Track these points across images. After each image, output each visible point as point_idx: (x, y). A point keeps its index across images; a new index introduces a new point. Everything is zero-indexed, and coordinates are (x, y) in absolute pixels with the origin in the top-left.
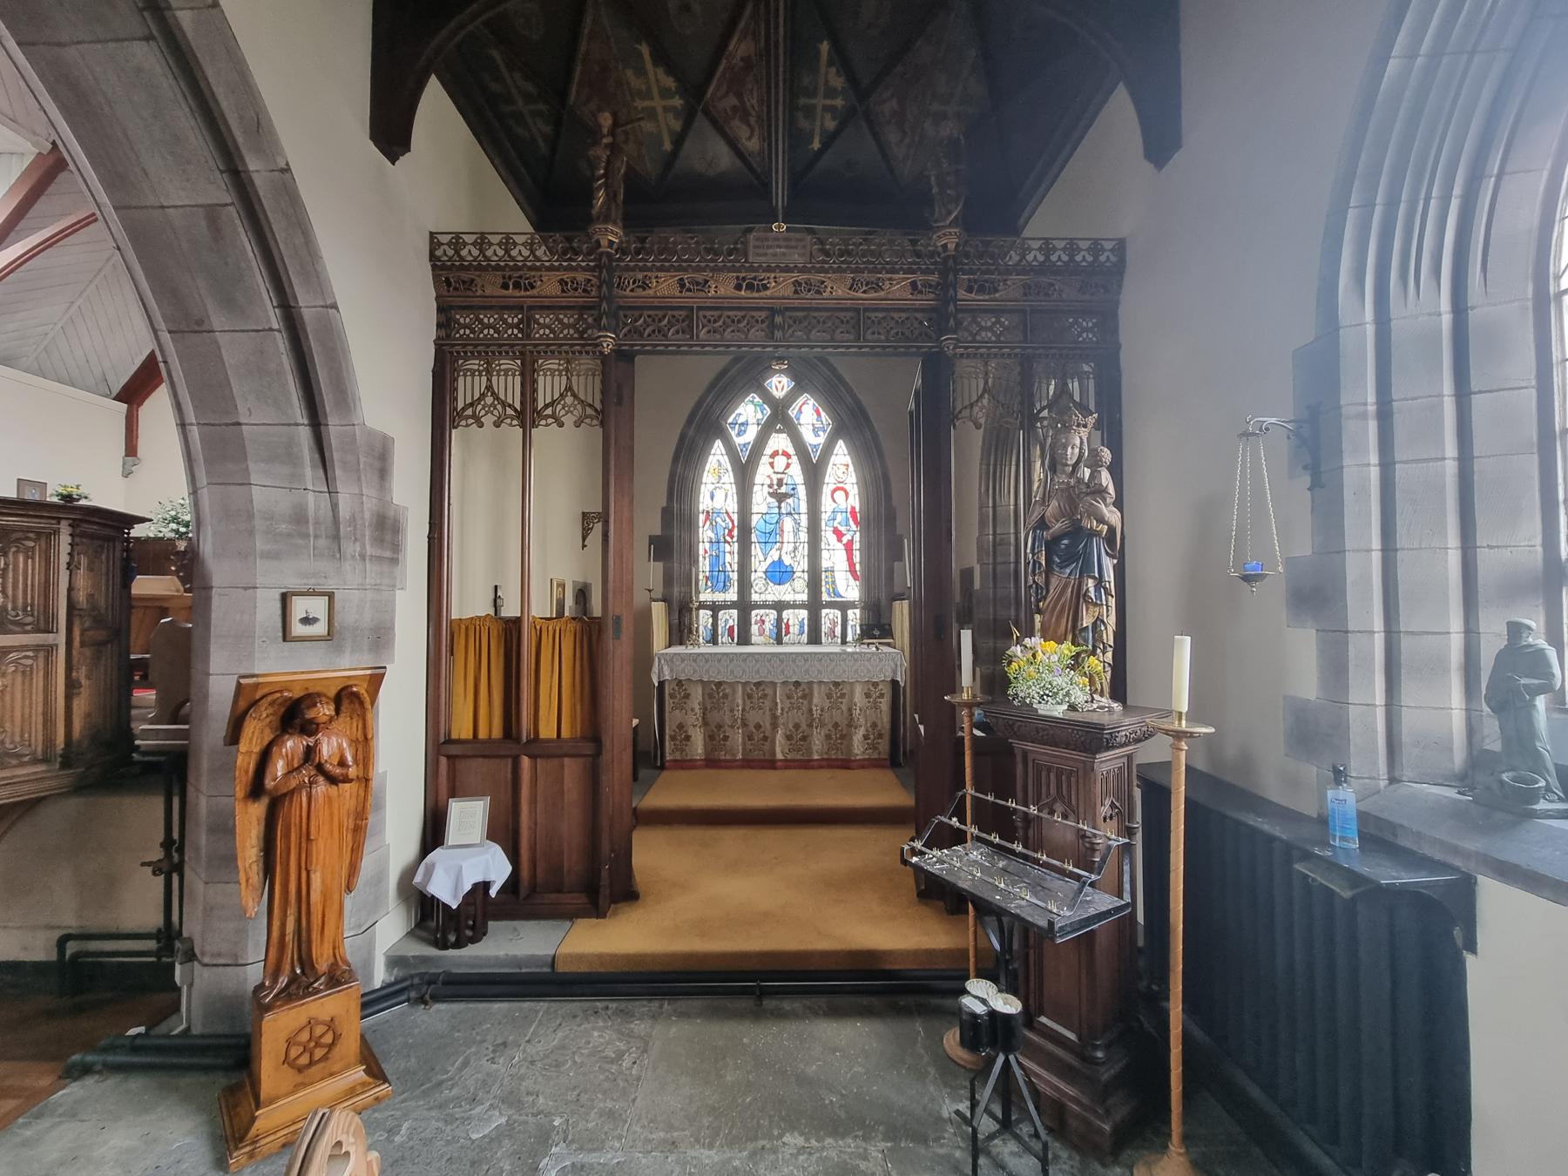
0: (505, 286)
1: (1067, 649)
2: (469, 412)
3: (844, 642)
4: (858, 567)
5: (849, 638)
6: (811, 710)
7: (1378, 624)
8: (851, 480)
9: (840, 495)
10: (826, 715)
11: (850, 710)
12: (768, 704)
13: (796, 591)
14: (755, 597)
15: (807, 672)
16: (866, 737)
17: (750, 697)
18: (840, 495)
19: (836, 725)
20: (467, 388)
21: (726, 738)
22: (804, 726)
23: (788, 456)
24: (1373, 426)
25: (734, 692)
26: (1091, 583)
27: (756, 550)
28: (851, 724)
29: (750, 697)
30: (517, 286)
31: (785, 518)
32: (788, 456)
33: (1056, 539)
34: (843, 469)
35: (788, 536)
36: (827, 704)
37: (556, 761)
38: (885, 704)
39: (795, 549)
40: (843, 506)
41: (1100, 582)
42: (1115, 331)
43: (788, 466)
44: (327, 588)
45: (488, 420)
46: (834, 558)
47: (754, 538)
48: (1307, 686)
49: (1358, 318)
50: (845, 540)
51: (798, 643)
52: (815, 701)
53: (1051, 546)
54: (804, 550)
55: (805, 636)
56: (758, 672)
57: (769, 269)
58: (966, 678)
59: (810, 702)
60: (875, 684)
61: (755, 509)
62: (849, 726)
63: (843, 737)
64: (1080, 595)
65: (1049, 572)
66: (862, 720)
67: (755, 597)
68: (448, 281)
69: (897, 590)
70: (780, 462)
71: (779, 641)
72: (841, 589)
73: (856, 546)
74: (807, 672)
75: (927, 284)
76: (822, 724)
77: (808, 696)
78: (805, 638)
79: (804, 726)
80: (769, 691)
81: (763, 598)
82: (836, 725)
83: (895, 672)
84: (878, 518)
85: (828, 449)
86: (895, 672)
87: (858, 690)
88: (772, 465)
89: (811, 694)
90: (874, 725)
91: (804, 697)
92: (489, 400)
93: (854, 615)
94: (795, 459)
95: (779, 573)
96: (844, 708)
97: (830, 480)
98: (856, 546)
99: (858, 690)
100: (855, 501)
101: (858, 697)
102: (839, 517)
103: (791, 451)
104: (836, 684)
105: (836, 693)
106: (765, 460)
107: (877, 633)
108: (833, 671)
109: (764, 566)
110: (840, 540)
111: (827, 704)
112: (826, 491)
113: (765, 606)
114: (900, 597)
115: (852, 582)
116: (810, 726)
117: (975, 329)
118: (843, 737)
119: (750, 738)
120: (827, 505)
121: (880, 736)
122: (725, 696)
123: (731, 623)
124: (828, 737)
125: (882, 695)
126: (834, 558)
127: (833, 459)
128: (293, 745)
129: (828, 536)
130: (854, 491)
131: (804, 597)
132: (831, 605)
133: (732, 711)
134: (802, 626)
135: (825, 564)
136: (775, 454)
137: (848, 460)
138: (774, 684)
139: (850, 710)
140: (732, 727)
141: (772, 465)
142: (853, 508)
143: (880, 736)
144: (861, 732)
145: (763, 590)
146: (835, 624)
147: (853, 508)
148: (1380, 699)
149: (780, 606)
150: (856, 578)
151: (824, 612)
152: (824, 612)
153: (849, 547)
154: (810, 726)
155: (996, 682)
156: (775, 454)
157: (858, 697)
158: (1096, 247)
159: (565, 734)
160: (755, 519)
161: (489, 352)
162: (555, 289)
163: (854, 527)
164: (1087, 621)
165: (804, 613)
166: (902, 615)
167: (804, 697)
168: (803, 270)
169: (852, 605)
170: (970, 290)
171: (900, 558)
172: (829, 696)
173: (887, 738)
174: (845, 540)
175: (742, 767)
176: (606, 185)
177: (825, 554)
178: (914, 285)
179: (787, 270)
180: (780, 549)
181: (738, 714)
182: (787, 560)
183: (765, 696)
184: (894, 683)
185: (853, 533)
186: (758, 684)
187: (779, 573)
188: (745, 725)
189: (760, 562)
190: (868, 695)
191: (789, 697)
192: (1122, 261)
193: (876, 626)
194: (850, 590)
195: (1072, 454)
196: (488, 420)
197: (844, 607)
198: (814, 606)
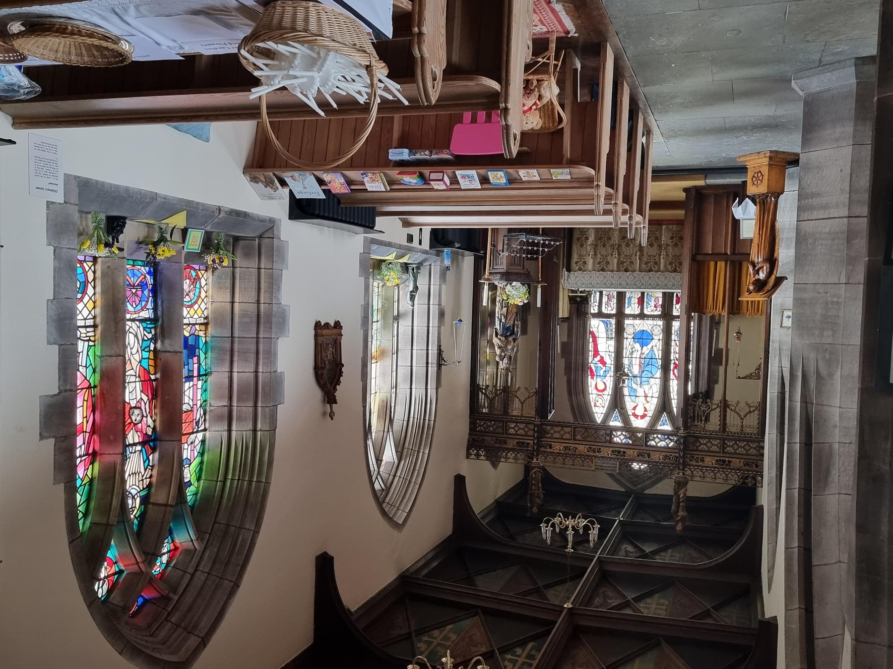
0: (729, 462)
1: (511, 301)
2: (752, 409)
3: (601, 293)
4: (591, 340)
5: (598, 294)
6: (619, 255)
7: (431, 307)
8: (593, 396)
9: (601, 387)
10: (610, 252)
11: (595, 255)
12: (645, 259)
13: (632, 326)
14: (660, 323)
15: (620, 277)
16: (587, 238)
17: (656, 263)
18: (601, 387)
19: (604, 246)
20: (752, 420)
21: (672, 238)
22: (623, 245)
23: (636, 416)
24: (430, 361)
25: (665, 266)
26: (503, 320)
27: (658, 354)
28: (595, 246)
29: (656, 263)
30: (724, 461)
31: (632, 372)
32: (636, 416)
33: (511, 335)
34: (598, 404)
35: (636, 362)
36: (609, 258)
37: (715, 252)
38: (575, 257)
39: (632, 353)
40: (599, 380)
41: (500, 321)
42: (471, 423)
43: (634, 408)
44: (782, 330)
45: (742, 404)
46: (606, 347)
47: (660, 362)
48: (443, 286)
49: (431, 392)
50: (598, 358)
51: (632, 296)
52: (616, 261)
53: (513, 333)
54: (626, 353)
55: (627, 296)
56: (650, 278)
57: (611, 458)
58: (539, 290)
59: (619, 260)
60: (580, 269)
61: (658, 381)
62: (596, 245)
63: (601, 238)
64: (506, 318)
65: (514, 325)
66: (589, 248)
67: (660, 323)
68: (757, 466)
69: (566, 325)
70: (640, 411)
71: (643, 294)
72: (602, 327)
73: (591, 354)
74: (620, 277)
75: (546, 448)
76: (612, 246)
77: (620, 263)
78: (628, 295)
79: (623, 245)
80: (644, 266)
81: (655, 322)
82: (604, 246)
83: (568, 277)
84: (578, 372)
85: (607, 416)
86: (568, 277)
87: (590, 266)
88: (646, 410)
89: (618, 264)
90: (582, 245)
91: (623, 263)
92: (742, 414)
93: (594, 309)
94: (630, 413)
95: (643, 338)
96: (599, 256)
97: (607, 398)
98: (591, 354)
99: (590, 266)
100: (591, 382)
101: (590, 262)
102: (602, 373)
103: (632, 418)
104: (603, 270)
105: (603, 265)
106: (650, 413)
107: (578, 299)
108: (605, 278)
109: (653, 343)
110: (602, 358)
111: (609, 258)
112: (609, 391)
113: (654, 317)
114: (564, 320)
115: (594, 330)
116: (620, 245)
117: (526, 429)
118: (601, 238)
119: (657, 238)
120: (610, 382)
121: (578, 239)
122: (671, 263)
123: (678, 306)
124: (609, 239)
125: (577, 263)
126: (606, 347)
127: (604, 411)
128: (762, 276)
129: (610, 361)
130: (591, 389)
131: (627, 322)
132: (609, 316)
133: (667, 255)
134: (629, 302)
135: (612, 343)
136: (643, 417)
137: (595, 410)
138: (640, 271)
139: (595, 255)
140: (667, 245)
141: (646, 410)
142: (592, 378)
143: (578, 239)
144: (590, 241)
145: (655, 327)
146: (607, 304)
147: (592, 378)
148: (432, 286)
149: (642, 316)
150: (592, 333)
151: (614, 312)
152: (614, 312)
153: (596, 353)
154: (620, 245)
155: (532, 293)
156: (643, 417)
157: (590, 262)
158: (478, 456)
159: (712, 264)
160: (658, 374)
161: (740, 437)
162: (707, 459)
163: (592, 366)
164: (505, 309)
165: (628, 311)
166: (563, 309)
167: (623, 263)
168: (596, 457)
169: (595, 316)
170: (528, 444)
171: (563, 344)
172: (608, 263)
173: (575, 239)
174: (598, 358)
175: (662, 220)
176: (679, 498)
177: (612, 349)
178: (551, 447)
179: (603, 457)
180: (642, 354)
181: (663, 253)
182: (637, 346)
183: (646, 263)
184: (569, 270)
185: (593, 362)
186: (650, 271)
187: (643, 338)
188: (660, 246)
189: (657, 344)
190: (585, 263)
191: (632, 263)
192: (468, 450)
193: (580, 303)
194: (596, 325)
195: (506, 360)
196: (742, 404)
197: (600, 315)
198: (620, 316)
